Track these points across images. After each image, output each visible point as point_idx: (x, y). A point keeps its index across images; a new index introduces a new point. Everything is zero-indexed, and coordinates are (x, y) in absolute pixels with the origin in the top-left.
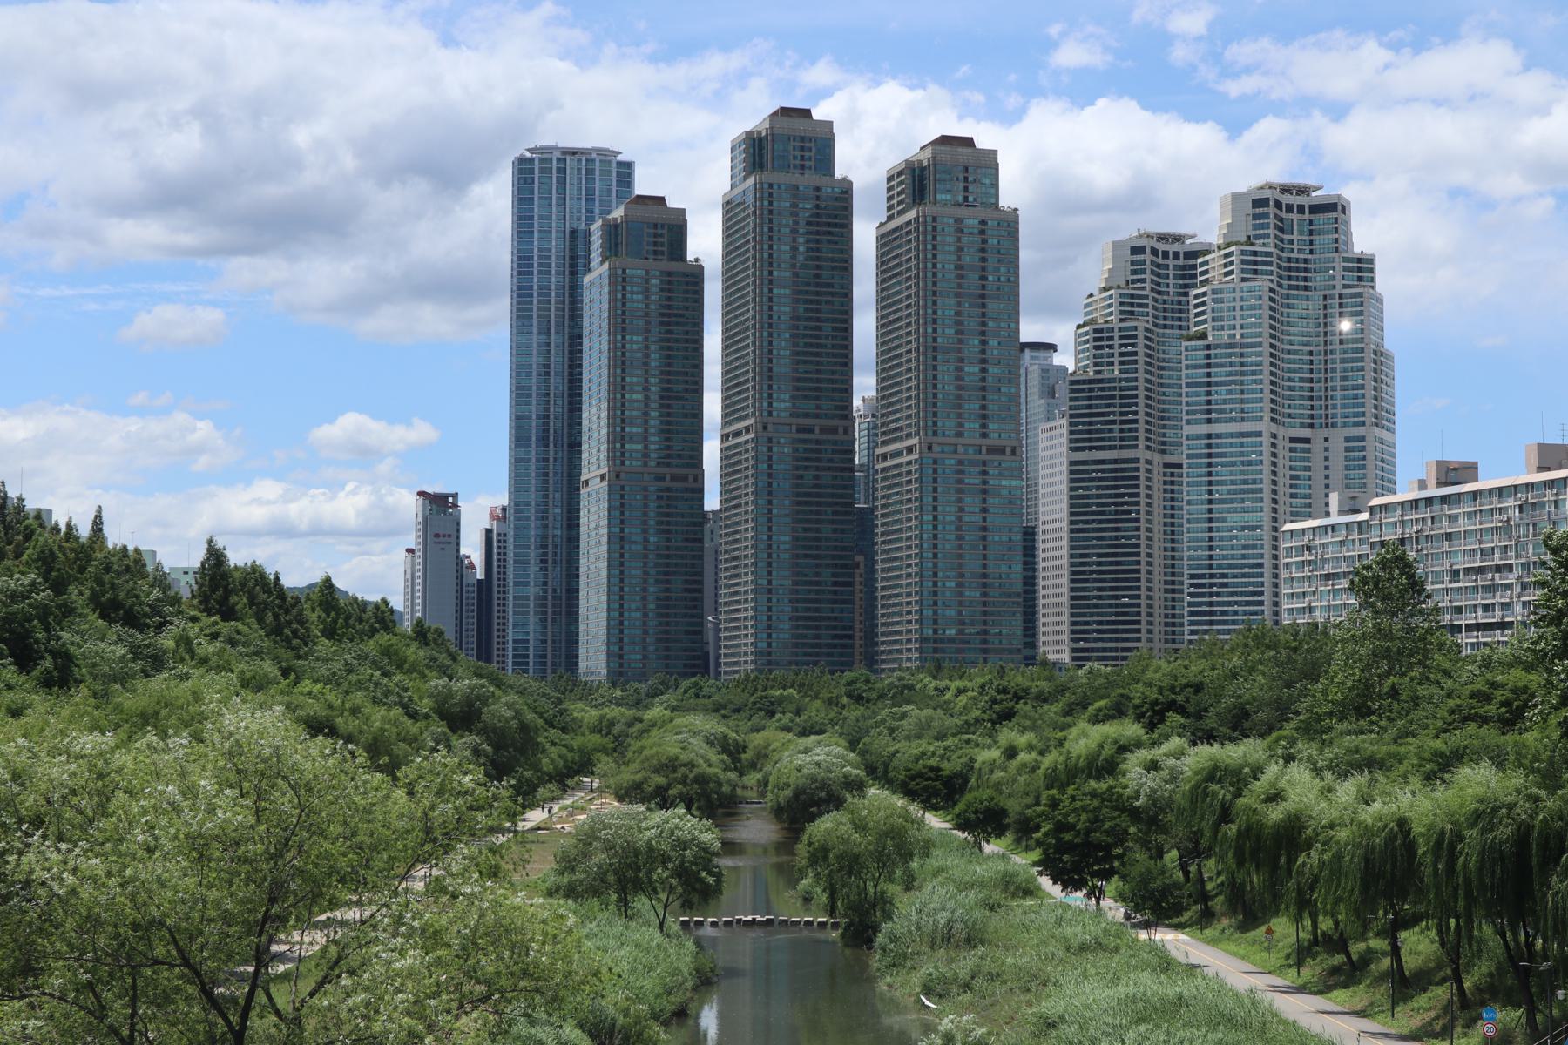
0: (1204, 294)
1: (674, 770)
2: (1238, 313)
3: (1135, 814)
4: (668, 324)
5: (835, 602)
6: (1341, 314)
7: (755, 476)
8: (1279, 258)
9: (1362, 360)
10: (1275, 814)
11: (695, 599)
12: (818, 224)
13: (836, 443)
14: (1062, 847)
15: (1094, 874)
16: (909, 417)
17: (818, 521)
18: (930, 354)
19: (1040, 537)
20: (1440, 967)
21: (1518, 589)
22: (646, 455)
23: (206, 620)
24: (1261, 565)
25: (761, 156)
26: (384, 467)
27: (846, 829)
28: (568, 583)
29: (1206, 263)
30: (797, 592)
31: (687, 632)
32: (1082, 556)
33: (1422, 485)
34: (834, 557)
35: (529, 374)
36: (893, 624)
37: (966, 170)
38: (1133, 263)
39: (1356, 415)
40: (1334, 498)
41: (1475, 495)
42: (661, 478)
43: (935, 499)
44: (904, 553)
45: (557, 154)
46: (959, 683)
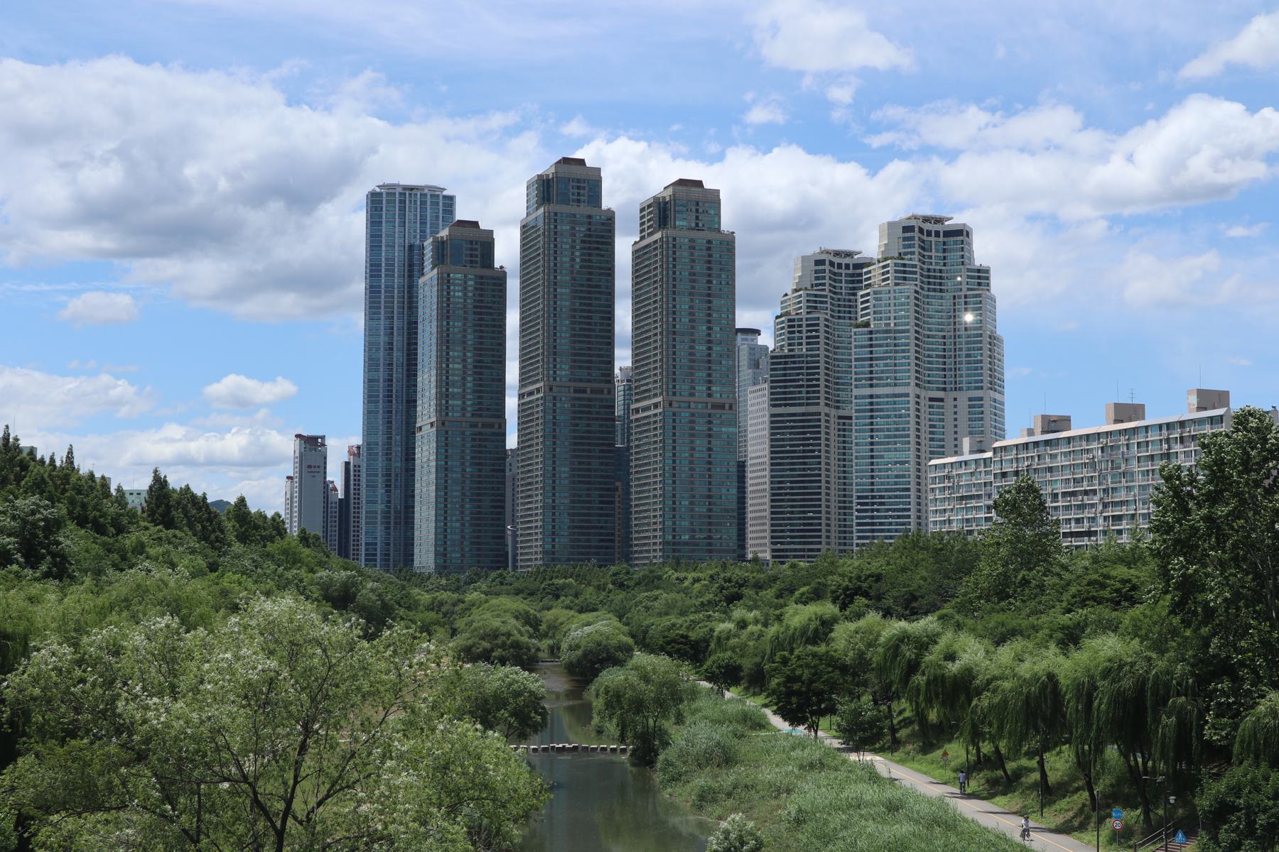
0: (868, 294)
1: (496, 637)
2: (892, 308)
3: (844, 669)
4: (481, 313)
5: (601, 515)
6: (966, 309)
7: (544, 424)
8: (922, 269)
9: (980, 342)
10: (954, 668)
11: (499, 513)
12: (590, 242)
13: (602, 400)
14: (790, 693)
15: (813, 713)
16: (655, 382)
17: (589, 457)
18: (671, 337)
19: (749, 469)
20: (1074, 779)
21: (1100, 508)
22: (463, 409)
23: (153, 529)
24: (908, 490)
25: (548, 192)
26: (262, 414)
27: (634, 678)
28: (406, 502)
29: (869, 272)
30: (573, 508)
31: (493, 537)
32: (779, 482)
33: (1031, 432)
34: (600, 483)
35: (378, 349)
36: (643, 531)
37: (697, 204)
38: (816, 272)
39: (976, 382)
40: (966, 443)
41: (1069, 440)
42: (474, 425)
43: (674, 441)
44: (652, 480)
45: (399, 190)
46: (694, 575)
